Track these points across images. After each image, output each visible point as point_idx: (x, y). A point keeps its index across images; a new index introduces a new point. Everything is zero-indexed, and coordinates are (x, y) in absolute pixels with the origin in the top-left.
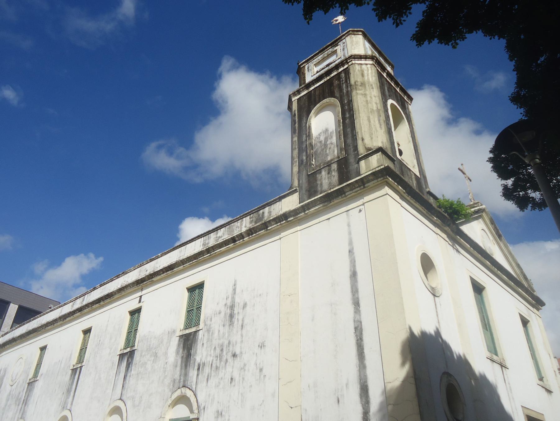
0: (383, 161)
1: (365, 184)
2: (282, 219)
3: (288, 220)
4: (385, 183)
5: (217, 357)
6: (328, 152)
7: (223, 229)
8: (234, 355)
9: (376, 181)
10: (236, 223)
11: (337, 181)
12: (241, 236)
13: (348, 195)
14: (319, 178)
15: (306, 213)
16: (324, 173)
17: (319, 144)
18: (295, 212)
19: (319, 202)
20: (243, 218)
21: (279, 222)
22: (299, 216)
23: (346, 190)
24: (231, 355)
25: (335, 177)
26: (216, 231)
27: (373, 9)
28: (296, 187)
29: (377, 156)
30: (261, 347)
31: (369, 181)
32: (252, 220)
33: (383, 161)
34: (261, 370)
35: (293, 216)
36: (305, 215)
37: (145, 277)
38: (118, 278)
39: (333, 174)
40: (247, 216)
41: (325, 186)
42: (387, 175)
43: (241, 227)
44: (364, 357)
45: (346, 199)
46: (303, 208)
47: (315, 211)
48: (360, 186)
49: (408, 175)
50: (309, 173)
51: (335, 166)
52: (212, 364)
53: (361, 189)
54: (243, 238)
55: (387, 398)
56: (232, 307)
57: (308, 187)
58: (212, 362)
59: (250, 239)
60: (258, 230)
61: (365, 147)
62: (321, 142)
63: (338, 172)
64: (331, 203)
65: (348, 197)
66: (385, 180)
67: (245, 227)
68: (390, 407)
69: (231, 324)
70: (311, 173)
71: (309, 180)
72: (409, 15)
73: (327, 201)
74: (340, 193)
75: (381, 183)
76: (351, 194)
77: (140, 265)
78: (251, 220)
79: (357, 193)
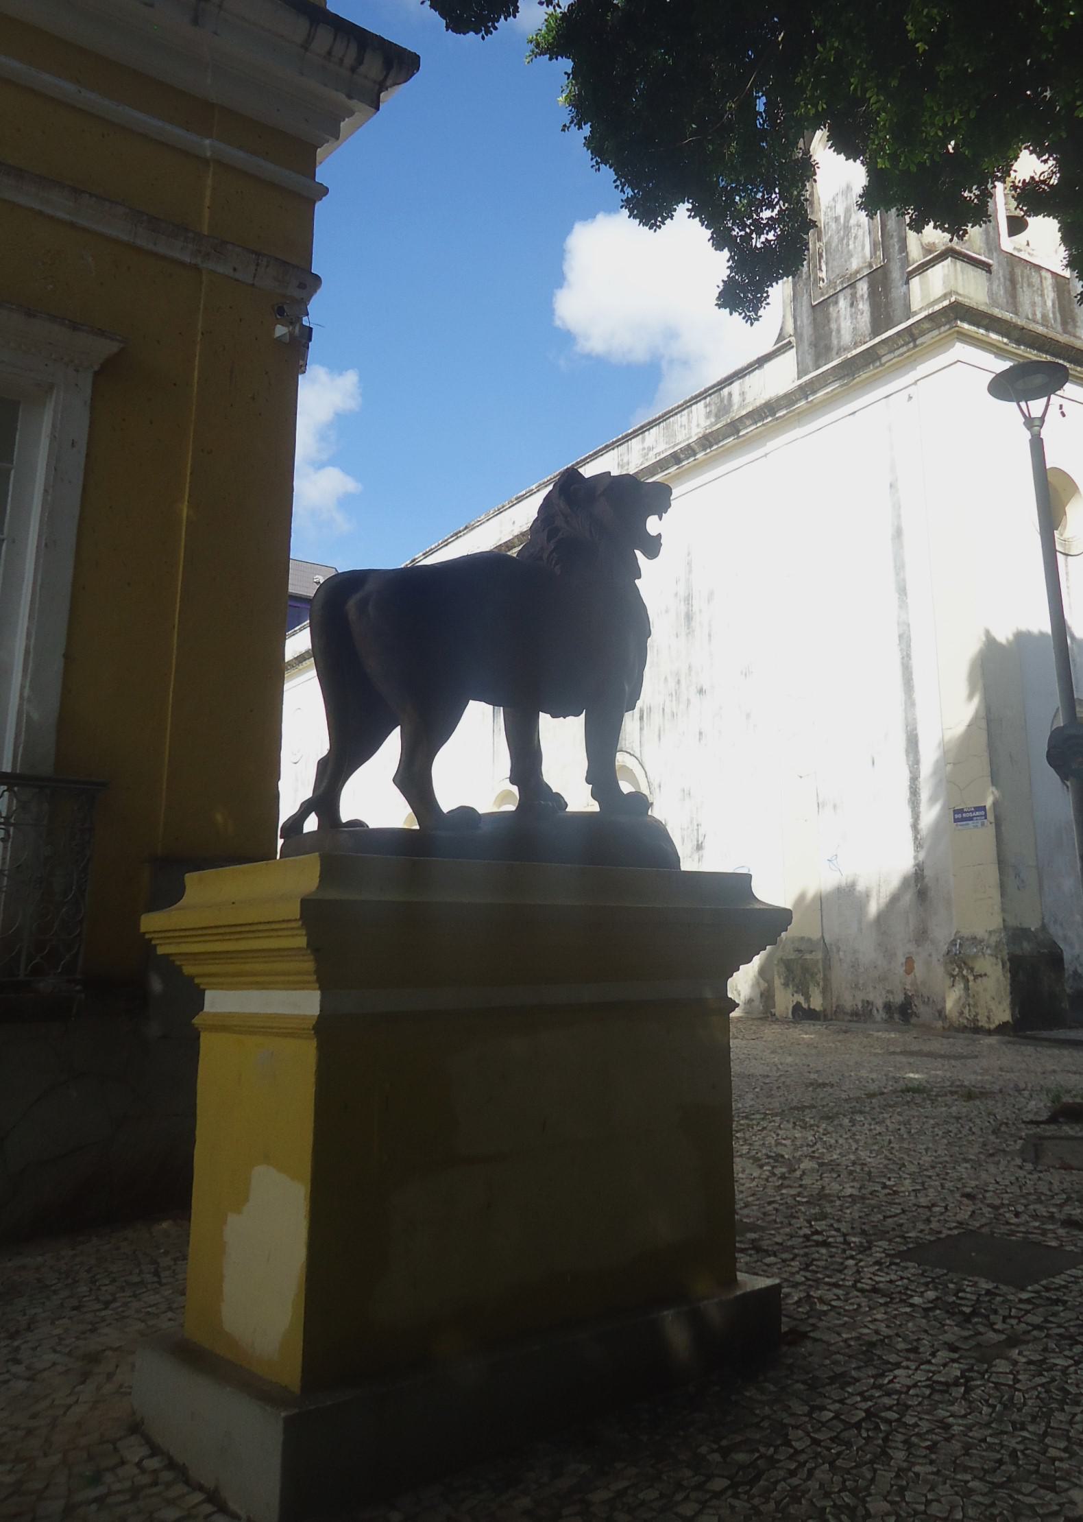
0: (956, 279)
1: (917, 339)
2: (765, 413)
3: (777, 416)
4: (955, 335)
5: (672, 694)
6: (851, 247)
7: (655, 428)
8: (701, 691)
9: (936, 332)
10: (679, 415)
11: (869, 325)
12: (690, 451)
13: (886, 362)
14: (834, 315)
15: (809, 400)
16: (843, 303)
17: (833, 225)
18: (788, 399)
19: (832, 379)
20: (691, 405)
21: (760, 421)
22: (796, 406)
23: (881, 352)
24: (695, 690)
25: (864, 314)
26: (642, 433)
27: (716, 305)
28: (790, 336)
29: (943, 266)
30: (746, 675)
31: (923, 333)
32: (710, 411)
33: (956, 279)
34: (748, 716)
35: (786, 407)
36: (809, 405)
37: (512, 539)
38: (457, 538)
39: (861, 306)
40: (700, 401)
41: (847, 338)
42: (956, 319)
43: (689, 425)
44: (913, 687)
45: (885, 369)
46: (804, 391)
47: (825, 397)
48: (907, 344)
49: (1030, 285)
50: (814, 301)
51: (863, 288)
52: (663, 709)
53: (908, 351)
54: (695, 454)
55: (945, 753)
56: (688, 599)
57: (813, 338)
58: (664, 704)
59: (709, 455)
60: (721, 438)
61: (921, 244)
62: (837, 219)
63: (870, 304)
64: (854, 379)
65: (887, 365)
66: (953, 330)
67: (698, 425)
68: (949, 767)
69: (689, 633)
70: (819, 303)
71: (815, 319)
72: (766, 306)
73: (848, 375)
74: (870, 357)
75: (946, 336)
76: (892, 359)
77: (499, 510)
78: (708, 410)
79: (903, 357)
